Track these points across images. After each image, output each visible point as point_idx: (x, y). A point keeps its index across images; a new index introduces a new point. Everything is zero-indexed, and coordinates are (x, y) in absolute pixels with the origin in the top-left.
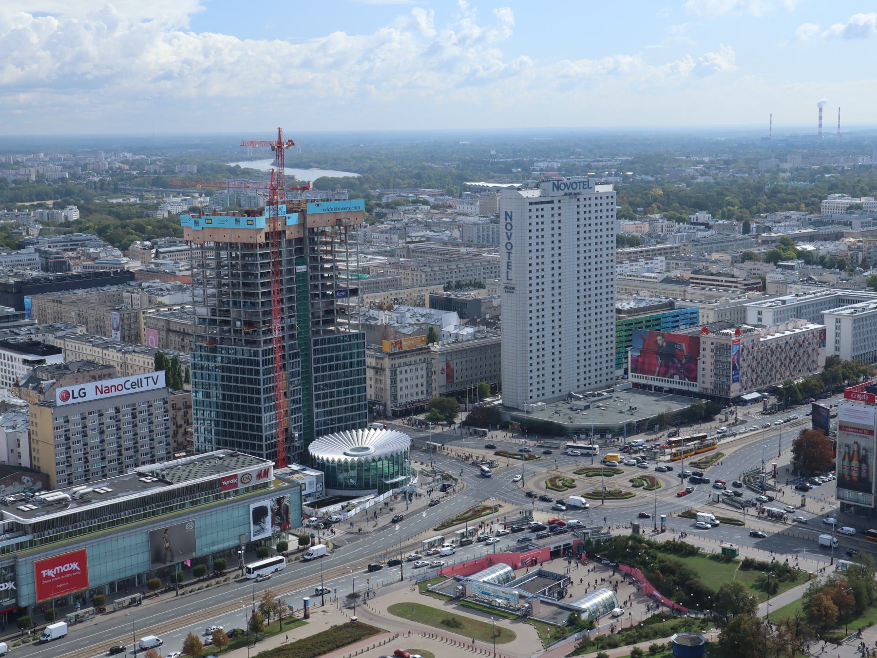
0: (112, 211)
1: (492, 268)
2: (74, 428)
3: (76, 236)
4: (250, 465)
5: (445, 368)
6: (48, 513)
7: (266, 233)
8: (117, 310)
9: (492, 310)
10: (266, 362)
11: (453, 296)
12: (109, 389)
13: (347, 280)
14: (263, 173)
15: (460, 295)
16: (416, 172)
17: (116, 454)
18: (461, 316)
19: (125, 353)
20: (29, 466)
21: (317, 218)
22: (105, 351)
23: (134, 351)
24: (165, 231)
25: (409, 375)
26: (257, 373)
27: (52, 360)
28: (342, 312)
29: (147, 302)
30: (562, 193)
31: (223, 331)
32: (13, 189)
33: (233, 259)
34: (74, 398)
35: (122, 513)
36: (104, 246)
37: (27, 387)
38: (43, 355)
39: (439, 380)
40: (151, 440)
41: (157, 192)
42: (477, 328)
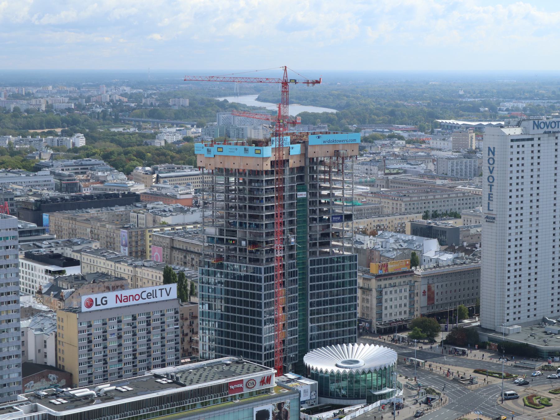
0: (113, 139)
1: (471, 200)
2: (96, 332)
3: (86, 161)
4: (254, 372)
5: (426, 290)
6: (76, 407)
7: (271, 162)
8: (126, 228)
9: (469, 238)
10: (267, 279)
11: (433, 225)
12: (127, 299)
13: (343, 206)
14: (248, 107)
15: (440, 224)
16: (390, 109)
17: (131, 357)
18: (441, 243)
19: (136, 267)
20: (54, 365)
21: (317, 149)
22: (117, 265)
23: (144, 266)
24: (163, 158)
25: (393, 296)
26: (260, 288)
27: (71, 271)
28: (337, 235)
29: (152, 222)
30: (541, 131)
31: (229, 249)
32: (26, 117)
33: (240, 184)
34: (97, 305)
35: (141, 411)
36: (111, 170)
37: (49, 294)
38: (64, 266)
39: (421, 301)
40: (162, 346)
41: (153, 122)
42: (456, 255)
